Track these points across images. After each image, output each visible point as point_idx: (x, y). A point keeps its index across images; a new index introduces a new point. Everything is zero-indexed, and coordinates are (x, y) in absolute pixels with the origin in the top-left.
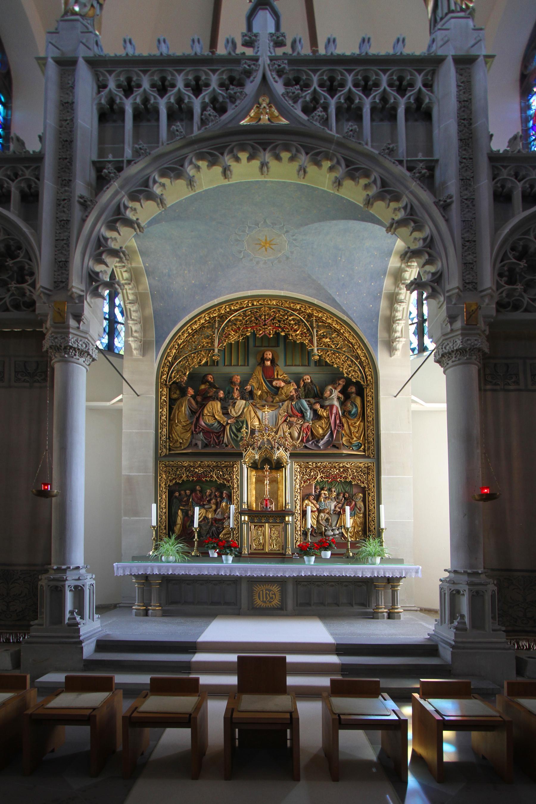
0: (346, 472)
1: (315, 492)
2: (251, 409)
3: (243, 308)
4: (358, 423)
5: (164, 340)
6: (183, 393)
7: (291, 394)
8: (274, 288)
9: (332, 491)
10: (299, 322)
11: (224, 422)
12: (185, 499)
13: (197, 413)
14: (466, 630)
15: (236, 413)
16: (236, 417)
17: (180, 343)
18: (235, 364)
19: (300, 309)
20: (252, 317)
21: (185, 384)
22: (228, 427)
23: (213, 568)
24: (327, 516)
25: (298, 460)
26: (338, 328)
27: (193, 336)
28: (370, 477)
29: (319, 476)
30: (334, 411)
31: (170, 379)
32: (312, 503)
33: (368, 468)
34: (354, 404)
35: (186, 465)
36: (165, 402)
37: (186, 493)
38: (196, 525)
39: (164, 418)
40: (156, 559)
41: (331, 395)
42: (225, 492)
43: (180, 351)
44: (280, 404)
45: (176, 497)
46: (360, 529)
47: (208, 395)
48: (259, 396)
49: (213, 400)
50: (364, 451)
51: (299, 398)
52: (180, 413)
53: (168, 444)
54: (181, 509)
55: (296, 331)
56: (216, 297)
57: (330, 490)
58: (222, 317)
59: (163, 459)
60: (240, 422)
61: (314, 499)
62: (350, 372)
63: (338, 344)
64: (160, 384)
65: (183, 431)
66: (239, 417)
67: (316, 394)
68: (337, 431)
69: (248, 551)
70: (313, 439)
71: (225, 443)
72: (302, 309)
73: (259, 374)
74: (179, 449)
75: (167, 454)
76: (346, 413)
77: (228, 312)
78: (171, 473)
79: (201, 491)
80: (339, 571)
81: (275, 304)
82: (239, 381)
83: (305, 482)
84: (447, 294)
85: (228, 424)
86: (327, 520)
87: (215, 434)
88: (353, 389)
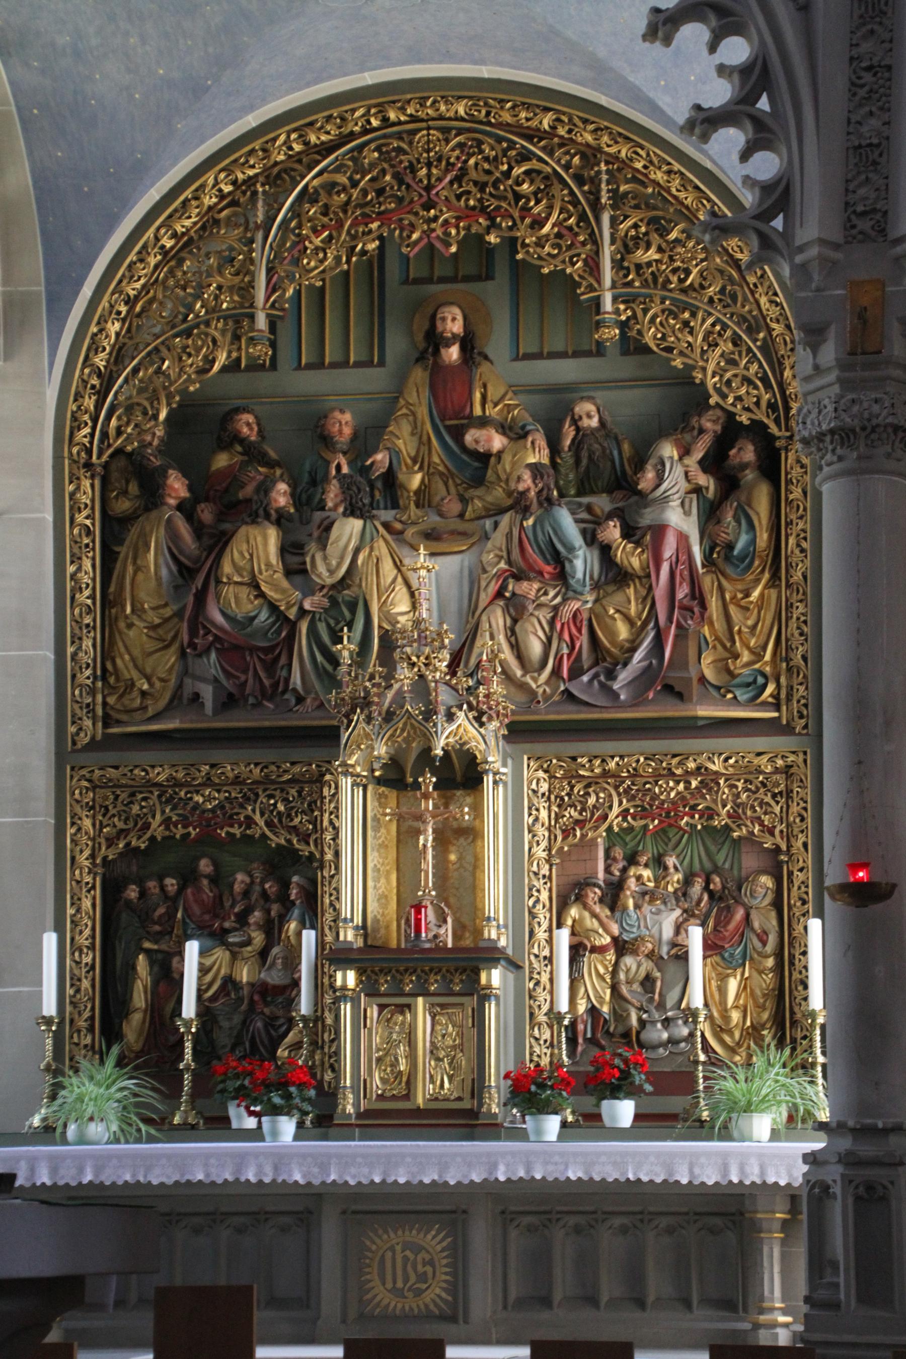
0: (710, 790)
1: (607, 870)
2: (384, 550)
3: (352, 136)
4: (756, 594)
5: (77, 293)
6: (152, 494)
7: (521, 487)
8: (448, 57)
9: (666, 868)
10: (548, 182)
11: (289, 606)
12: (161, 910)
13: (198, 570)
14: (835, 1306)
15: (332, 572)
16: (333, 587)
17: (132, 293)
18: (339, 358)
19: (553, 128)
20: (384, 172)
21: (160, 451)
22: (304, 627)
23: (220, 1156)
24: (647, 965)
25: (539, 748)
26: (688, 202)
27: (180, 262)
28: (794, 809)
29: (616, 810)
30: (669, 550)
31: (101, 441)
32: (594, 915)
33: (787, 771)
34: (744, 516)
35: (161, 778)
36: (89, 532)
37: (162, 888)
38: (189, 1008)
39: (83, 597)
40: (49, 1132)
41: (658, 486)
42: (295, 879)
43: (133, 322)
44: (488, 524)
45: (128, 902)
46: (765, 1016)
47: (241, 496)
48: (417, 492)
49: (254, 522)
50: (777, 707)
51: (546, 502)
52: (140, 576)
53: (99, 698)
54: (148, 952)
55: (538, 223)
56: (252, 108)
57: (658, 863)
58: (279, 178)
59: (83, 759)
60: (345, 601)
61: (601, 901)
62: (729, 383)
63: (688, 272)
64: (70, 463)
65: (150, 646)
66: (343, 583)
67: (610, 478)
68: (679, 626)
69: (356, 1105)
70: (596, 663)
71: (295, 690)
72: (562, 131)
73: (418, 396)
74: (138, 716)
75: (99, 737)
76: (720, 555)
77: (297, 158)
78: (112, 811)
79: (214, 880)
80: (615, 1164)
81: (461, 112)
82: (347, 431)
83: (566, 833)
84: (799, 259)
85: (302, 612)
86: (648, 982)
87: (258, 657)
88: (746, 453)
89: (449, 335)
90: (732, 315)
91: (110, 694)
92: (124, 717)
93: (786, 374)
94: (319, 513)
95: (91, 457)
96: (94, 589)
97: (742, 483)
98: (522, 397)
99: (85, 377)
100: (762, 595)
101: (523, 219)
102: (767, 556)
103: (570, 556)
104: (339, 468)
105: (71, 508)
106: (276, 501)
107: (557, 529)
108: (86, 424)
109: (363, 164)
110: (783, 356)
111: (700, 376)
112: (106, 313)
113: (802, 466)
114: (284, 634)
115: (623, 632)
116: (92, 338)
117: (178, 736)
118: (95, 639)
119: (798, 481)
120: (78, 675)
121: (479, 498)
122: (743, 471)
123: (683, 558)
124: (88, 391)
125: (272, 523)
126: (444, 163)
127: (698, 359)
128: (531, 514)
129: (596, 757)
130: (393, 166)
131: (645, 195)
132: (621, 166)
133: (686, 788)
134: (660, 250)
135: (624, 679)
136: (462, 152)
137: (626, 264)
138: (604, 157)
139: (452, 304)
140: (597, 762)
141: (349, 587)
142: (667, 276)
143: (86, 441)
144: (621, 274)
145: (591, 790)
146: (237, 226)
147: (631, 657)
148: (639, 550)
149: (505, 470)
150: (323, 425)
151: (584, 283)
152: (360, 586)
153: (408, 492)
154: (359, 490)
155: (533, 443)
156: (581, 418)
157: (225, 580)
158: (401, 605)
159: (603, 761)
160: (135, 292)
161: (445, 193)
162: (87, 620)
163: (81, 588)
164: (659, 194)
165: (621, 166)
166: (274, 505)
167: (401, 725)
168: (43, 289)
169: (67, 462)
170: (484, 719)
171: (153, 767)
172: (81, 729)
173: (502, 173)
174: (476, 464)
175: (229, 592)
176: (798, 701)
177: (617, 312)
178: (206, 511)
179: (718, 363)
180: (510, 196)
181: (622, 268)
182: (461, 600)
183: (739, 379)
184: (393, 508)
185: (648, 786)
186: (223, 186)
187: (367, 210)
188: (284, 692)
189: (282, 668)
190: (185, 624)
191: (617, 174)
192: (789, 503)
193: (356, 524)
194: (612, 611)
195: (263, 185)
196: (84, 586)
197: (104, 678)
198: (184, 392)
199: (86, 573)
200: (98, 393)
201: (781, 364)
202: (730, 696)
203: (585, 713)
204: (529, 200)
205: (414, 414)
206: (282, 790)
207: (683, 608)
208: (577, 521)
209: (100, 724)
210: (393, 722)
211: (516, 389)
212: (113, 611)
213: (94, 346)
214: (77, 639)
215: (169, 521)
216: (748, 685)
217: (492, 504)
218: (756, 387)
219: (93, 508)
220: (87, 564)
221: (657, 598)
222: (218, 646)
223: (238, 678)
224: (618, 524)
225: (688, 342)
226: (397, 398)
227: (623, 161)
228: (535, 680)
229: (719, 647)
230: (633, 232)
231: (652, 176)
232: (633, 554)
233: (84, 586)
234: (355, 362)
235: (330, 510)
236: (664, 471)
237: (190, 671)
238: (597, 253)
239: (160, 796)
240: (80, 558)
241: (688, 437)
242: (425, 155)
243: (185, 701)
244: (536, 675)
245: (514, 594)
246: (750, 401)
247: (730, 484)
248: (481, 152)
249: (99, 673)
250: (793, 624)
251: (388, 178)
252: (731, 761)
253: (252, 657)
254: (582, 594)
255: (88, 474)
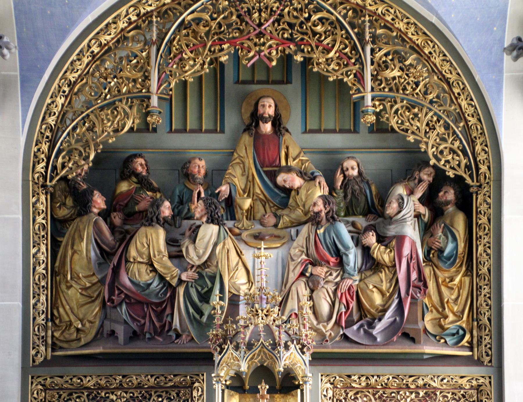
5: (41, 78)
6: (83, 205)
7: (316, 209)
11: (172, 278)
13: (114, 254)
15: (199, 257)
16: (199, 266)
17: (73, 80)
20: (231, 14)
22: (181, 291)
25: (328, 369)
26: (419, 42)
27: (103, 61)
30: (406, 250)
31: (52, 171)
34: (449, 231)
39: (40, 269)
41: (399, 212)
44: (293, 231)
47: (137, 208)
48: (247, 211)
49: (150, 225)
50: (471, 349)
51: (332, 219)
52: (76, 257)
53: (50, 333)
62: (442, 152)
65: (82, 300)
66: (205, 265)
67: (368, 206)
68: (413, 298)
70: (360, 319)
71: (176, 330)
74: (74, 344)
76: (434, 255)
82: (203, 171)
85: (180, 282)
87: (153, 307)
88: (449, 195)
89: (267, 116)
90: (444, 111)
91: (55, 330)
92: (65, 345)
93: (477, 148)
94: (186, 221)
95: (46, 181)
96: (47, 264)
97: (445, 213)
98: (308, 155)
99: (43, 131)
100: (461, 281)
101: (317, 47)
102: (464, 257)
103: (347, 252)
104: (199, 194)
105: (34, 213)
106: (163, 212)
107: (338, 236)
108: (43, 160)
109: (219, 8)
110: (475, 137)
111: (424, 147)
112: (56, 92)
113: (487, 204)
114: (168, 295)
115: (378, 300)
116: (47, 107)
117: (101, 357)
118: (47, 295)
119: (485, 213)
120: (38, 318)
121: (287, 215)
122: (448, 205)
123: (414, 256)
124: (45, 140)
125: (161, 226)
126: (269, 10)
127: (423, 136)
128: (322, 226)
129: (362, 376)
130: (237, 10)
131: (391, 36)
132: (378, 18)
133: (416, 397)
134: (401, 69)
135: (379, 329)
136: (280, 4)
137: (379, 78)
138: (367, 12)
139: (268, 97)
140: (363, 379)
141: (209, 267)
142: (405, 86)
143: (43, 171)
144: (377, 83)
145: (358, 396)
146: (138, 42)
147: (384, 315)
148: (389, 250)
149: (302, 200)
150: (188, 167)
151: (355, 88)
152: (217, 266)
153: (241, 209)
154: (216, 208)
155: (319, 183)
156: (347, 169)
157: (132, 260)
158: (241, 278)
159: (367, 378)
160: (74, 79)
161: (270, 28)
162: (43, 283)
163: (39, 263)
164: (400, 36)
165: (378, 18)
166: (162, 215)
167: (257, 351)
168: (18, 73)
169: (31, 183)
170: (305, 350)
171: (85, 377)
172: (38, 352)
173: (305, 18)
174: (283, 195)
175: (134, 268)
176: (486, 346)
177: (374, 106)
178: (117, 218)
179: (436, 140)
180: (309, 32)
181: (377, 80)
182: (277, 276)
183: (448, 150)
184: (231, 219)
185: (393, 395)
186: (131, 16)
187: (221, 36)
188: (168, 331)
189: (167, 316)
190: (107, 287)
191: (375, 22)
192: (479, 226)
193: (215, 228)
194: (371, 287)
195: (156, 17)
196: (41, 262)
197: (52, 320)
198: (105, 143)
199: (43, 253)
200: (50, 141)
201: (473, 142)
202: (442, 341)
203: (357, 348)
204: (321, 36)
205: (243, 163)
206: (167, 392)
207: (415, 287)
208: (350, 232)
209: (50, 350)
210: (253, 350)
211: (304, 150)
212: (58, 278)
213: (49, 112)
214: (36, 295)
215: (96, 222)
216: (453, 335)
217: (295, 219)
218: (458, 155)
219: (47, 214)
220: (43, 248)
221: (400, 280)
222: (127, 301)
223: (139, 321)
224: (375, 234)
225: (417, 126)
226: (233, 153)
227: (379, 15)
228: (325, 327)
229: (434, 311)
230: (384, 59)
231: (397, 25)
232: (385, 252)
233: (41, 262)
234: (205, 130)
235: (197, 219)
236: (403, 203)
237: (108, 317)
238: (363, 70)
239: (88, 396)
240: (39, 244)
241: (412, 184)
242: (258, 5)
243: (105, 335)
244: (325, 324)
245: (311, 274)
246: (455, 164)
247: (437, 211)
248: (292, 4)
249: (49, 317)
250: (481, 299)
251: (234, 17)
252: (445, 381)
253: (148, 308)
254: (353, 276)
255: (44, 192)
